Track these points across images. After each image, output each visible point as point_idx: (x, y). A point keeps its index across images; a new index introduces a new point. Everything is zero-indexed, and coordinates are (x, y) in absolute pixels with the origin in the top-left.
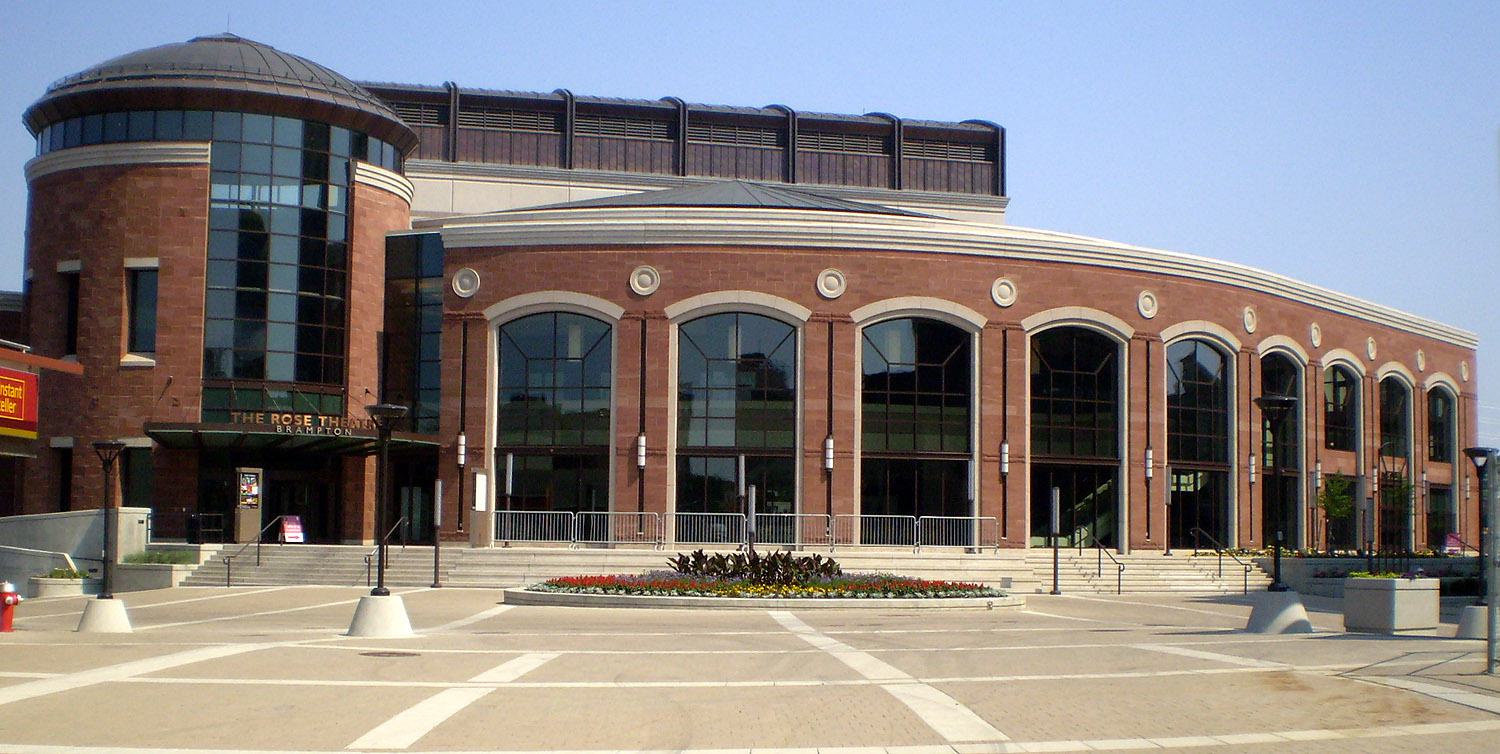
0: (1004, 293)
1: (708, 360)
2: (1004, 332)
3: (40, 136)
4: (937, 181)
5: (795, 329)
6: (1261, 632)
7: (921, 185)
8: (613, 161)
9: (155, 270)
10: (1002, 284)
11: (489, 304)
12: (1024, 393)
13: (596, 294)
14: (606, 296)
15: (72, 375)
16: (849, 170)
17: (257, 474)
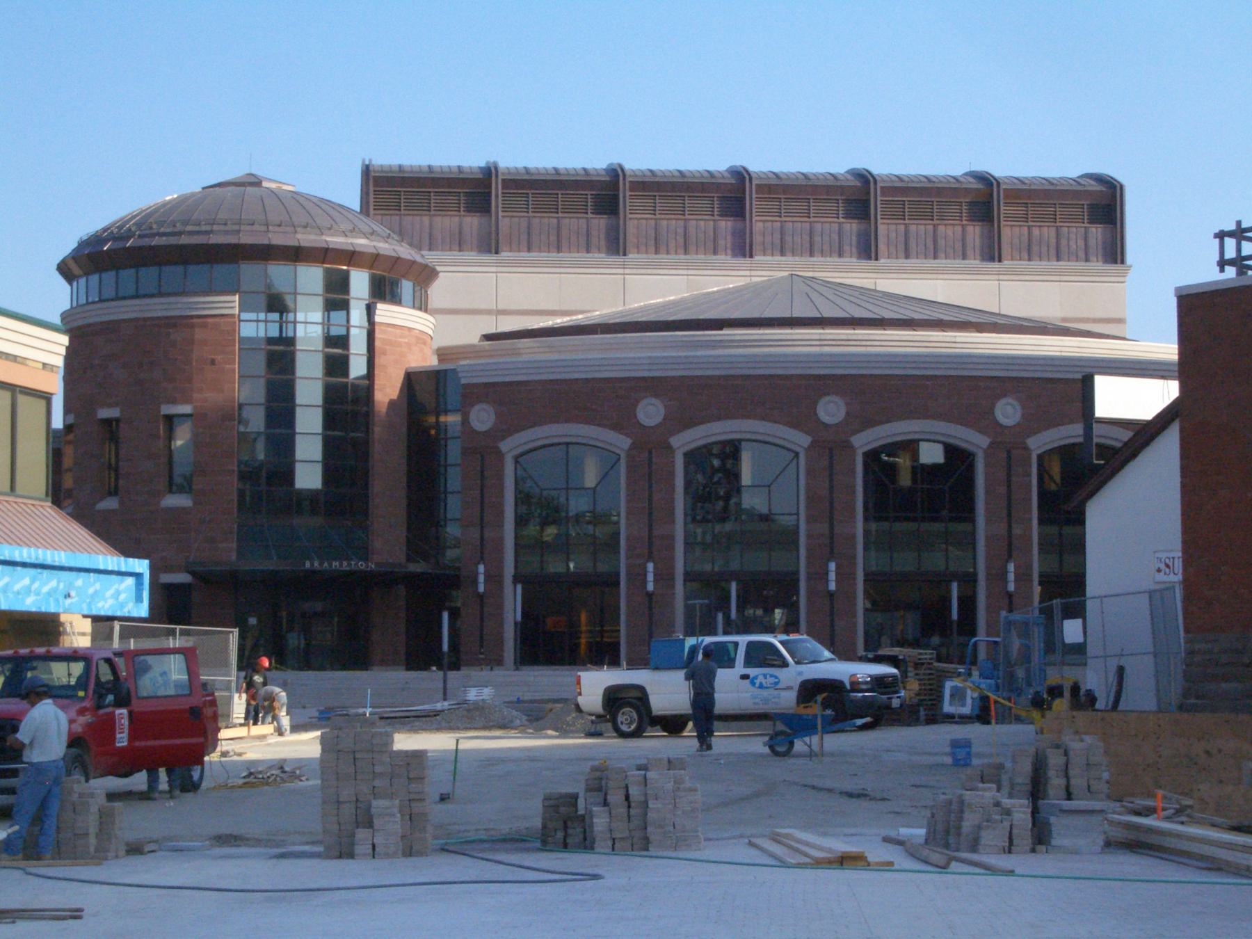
0: (1008, 412)
1: (769, 486)
2: (1009, 452)
3: (75, 284)
4: (1044, 249)
5: (797, 454)
6: (367, 670)
7: (902, 254)
8: (672, 245)
9: (117, 420)
10: (1006, 404)
11: (503, 438)
12: (1030, 511)
13: (604, 426)
15: (184, 508)
16: (817, 239)
17: (138, 576)
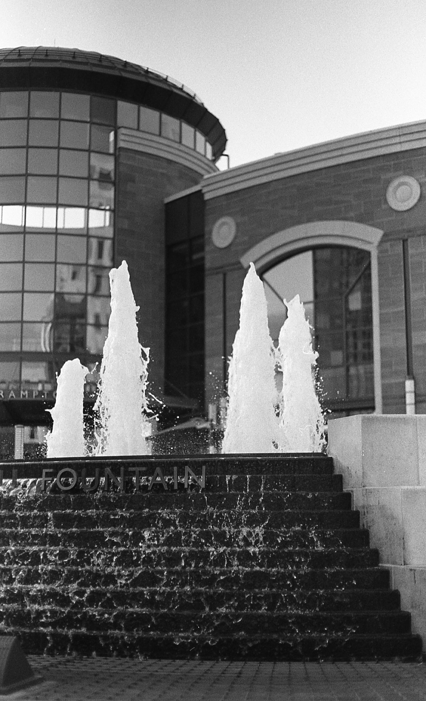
14: (360, 219)
